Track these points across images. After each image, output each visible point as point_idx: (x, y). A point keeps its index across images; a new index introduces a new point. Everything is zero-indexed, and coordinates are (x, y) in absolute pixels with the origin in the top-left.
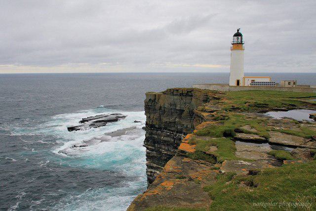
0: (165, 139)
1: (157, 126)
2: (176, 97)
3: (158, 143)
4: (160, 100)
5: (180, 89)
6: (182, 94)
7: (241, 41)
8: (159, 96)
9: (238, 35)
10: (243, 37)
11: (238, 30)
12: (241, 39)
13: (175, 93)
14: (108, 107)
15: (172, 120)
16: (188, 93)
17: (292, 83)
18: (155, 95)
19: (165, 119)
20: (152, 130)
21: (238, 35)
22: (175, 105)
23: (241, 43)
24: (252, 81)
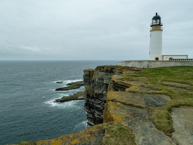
0: (97, 106)
1: (91, 96)
2: (103, 73)
3: (93, 108)
4: (94, 76)
5: (105, 66)
6: (107, 71)
7: (160, 22)
8: (93, 71)
9: (157, 17)
10: (161, 20)
11: (157, 14)
12: (160, 21)
13: (102, 70)
14: (70, 79)
15: (100, 92)
16: (110, 70)
17: (128, 74)
18: (90, 71)
19: (96, 91)
20: (88, 98)
21: (157, 17)
22: (103, 79)
23: (160, 25)
24: (170, 58)
